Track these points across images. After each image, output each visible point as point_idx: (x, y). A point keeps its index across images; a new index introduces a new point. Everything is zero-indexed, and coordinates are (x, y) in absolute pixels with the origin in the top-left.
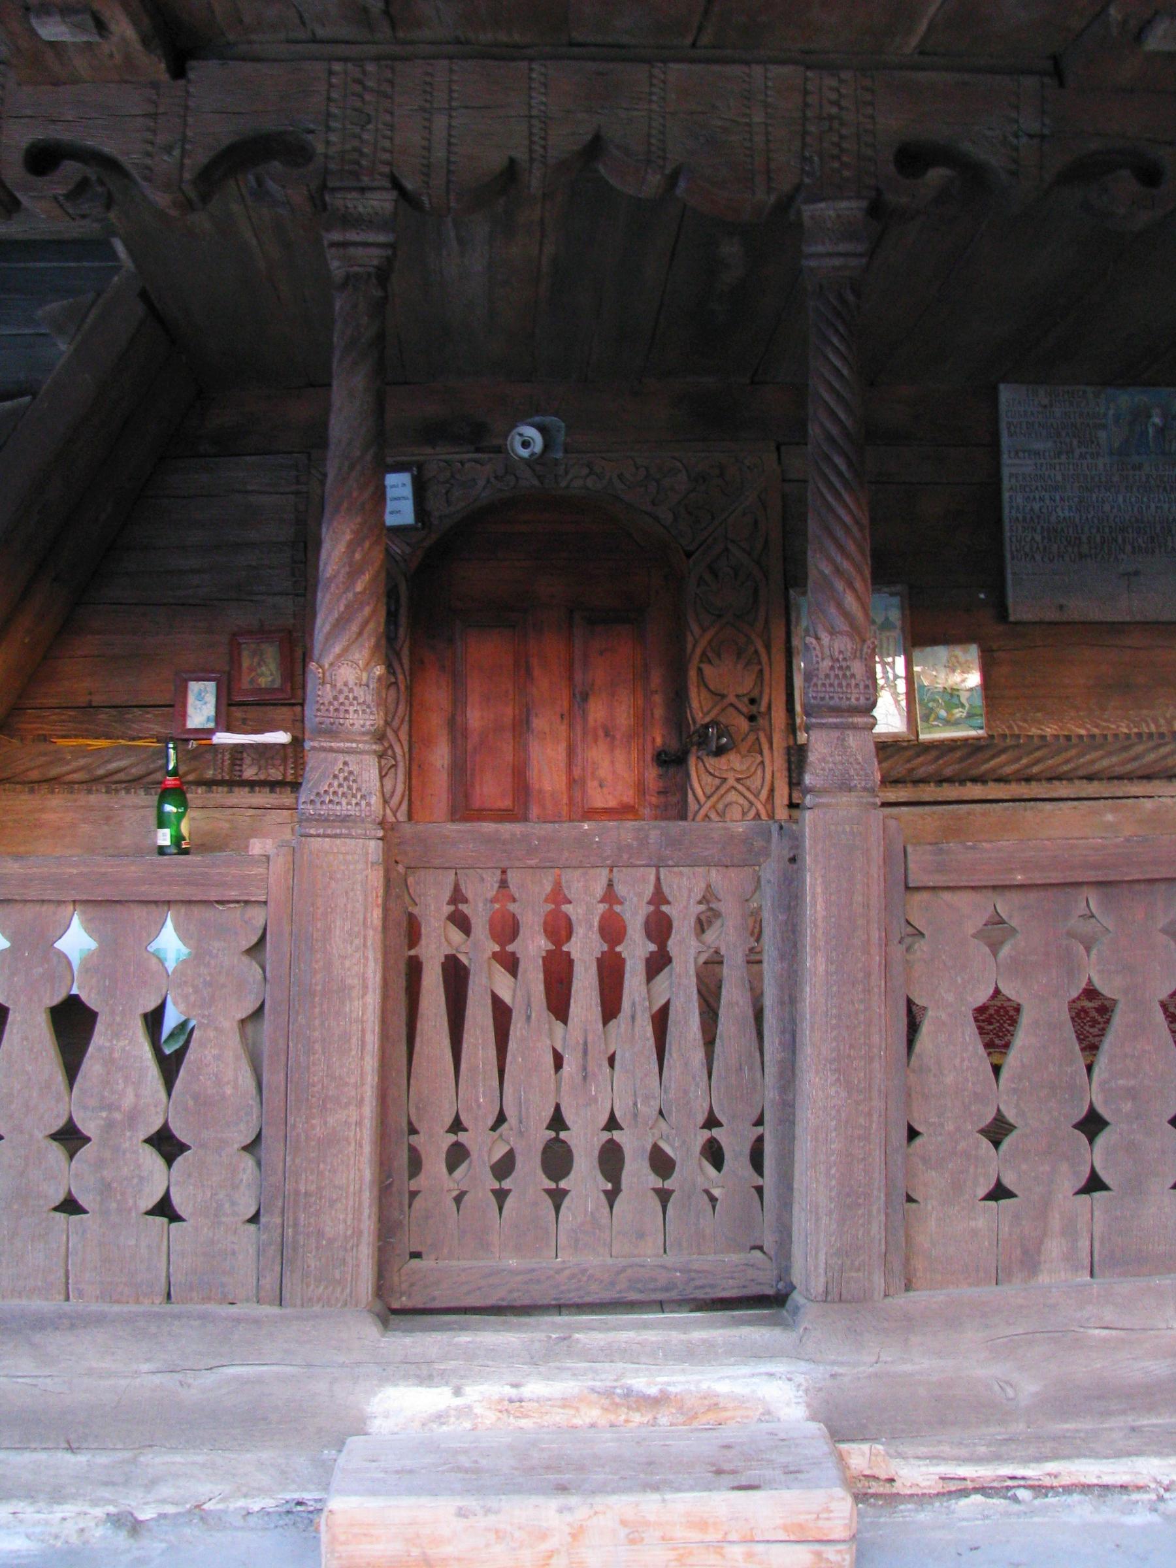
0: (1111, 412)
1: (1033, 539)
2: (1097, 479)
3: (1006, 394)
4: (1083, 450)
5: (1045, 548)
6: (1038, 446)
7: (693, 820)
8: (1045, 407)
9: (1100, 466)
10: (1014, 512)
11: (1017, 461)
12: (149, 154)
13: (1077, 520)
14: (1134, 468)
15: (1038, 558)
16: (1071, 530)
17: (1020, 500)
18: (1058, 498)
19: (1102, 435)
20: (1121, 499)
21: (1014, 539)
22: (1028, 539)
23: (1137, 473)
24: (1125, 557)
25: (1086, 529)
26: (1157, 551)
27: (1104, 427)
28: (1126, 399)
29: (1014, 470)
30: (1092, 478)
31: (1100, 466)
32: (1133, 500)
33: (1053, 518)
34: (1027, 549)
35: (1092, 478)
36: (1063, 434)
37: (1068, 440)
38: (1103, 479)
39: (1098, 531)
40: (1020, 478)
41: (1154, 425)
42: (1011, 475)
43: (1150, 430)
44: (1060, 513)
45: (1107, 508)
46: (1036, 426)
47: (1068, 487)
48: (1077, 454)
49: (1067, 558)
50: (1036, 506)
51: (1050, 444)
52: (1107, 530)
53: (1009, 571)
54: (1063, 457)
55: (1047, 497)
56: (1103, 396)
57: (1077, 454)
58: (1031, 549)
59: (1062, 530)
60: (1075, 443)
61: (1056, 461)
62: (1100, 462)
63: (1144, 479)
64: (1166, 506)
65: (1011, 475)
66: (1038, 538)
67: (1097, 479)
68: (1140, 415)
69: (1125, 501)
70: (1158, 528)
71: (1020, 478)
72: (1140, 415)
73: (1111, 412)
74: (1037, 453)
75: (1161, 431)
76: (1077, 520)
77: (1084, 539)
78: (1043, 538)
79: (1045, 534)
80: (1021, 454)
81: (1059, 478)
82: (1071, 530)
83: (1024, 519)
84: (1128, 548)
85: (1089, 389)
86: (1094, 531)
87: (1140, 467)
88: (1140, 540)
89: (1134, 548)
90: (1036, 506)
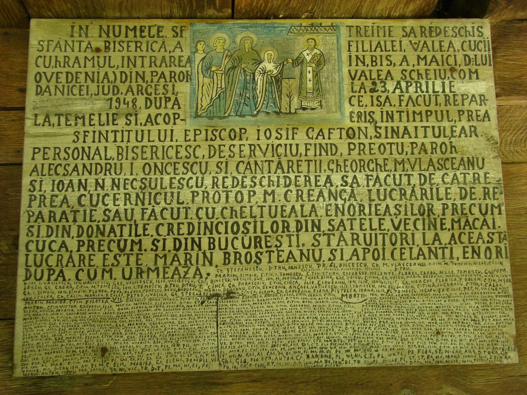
0: (199, 57)
1: (64, 245)
2: (172, 153)
3: (39, 31)
4: (153, 111)
5: (82, 259)
6: (81, 106)
7: (53, 73)
8: (98, 50)
9: (179, 135)
10: (35, 204)
11: (47, 129)
12: (499, 252)
13: (137, 216)
14: (233, 135)
15: (69, 273)
16: (126, 230)
17: (47, 187)
18: (108, 183)
19: (184, 88)
20: (208, 181)
21: (32, 247)
22: (55, 247)
23: (237, 142)
24: (212, 270)
25: (151, 230)
26: (265, 258)
27: (187, 77)
28: (222, 37)
29: (41, 143)
30: (165, 151)
31: (179, 135)
32: (229, 182)
33: (98, 215)
34: (52, 261)
35: (165, 151)
36: (123, 88)
37: (129, 98)
38: (183, 153)
39: (170, 230)
40: (51, 154)
41: (264, 72)
42: (36, 150)
43: (259, 78)
44: (111, 206)
45: (186, 195)
46: (82, 77)
47: (126, 164)
48: (142, 117)
49: (117, 273)
50: (73, 196)
51: (100, 104)
52: (184, 229)
53: (20, 296)
54: (121, 121)
55: (91, 181)
56: (187, 34)
57: (142, 117)
58: (59, 261)
59: (112, 230)
60: (141, 101)
61: (111, 128)
62: (179, 129)
63: (246, 151)
64: (281, 191)
65: (36, 150)
66: (72, 244)
67: (172, 153)
68: (240, 61)
69: (215, 184)
70: (267, 227)
71: (51, 154)
72: (240, 61)
73: (199, 57)
74: (79, 117)
75: (277, 81)
76: (137, 216)
77: (147, 243)
78: (80, 244)
79: (84, 238)
80: (54, 120)
81: (112, 152)
82: (126, 230)
83: (52, 216)
84: (218, 256)
85: (168, 25)
86: (164, 230)
87: (241, 134)
88: (238, 244)
89: (227, 254)
90: (73, 196)
